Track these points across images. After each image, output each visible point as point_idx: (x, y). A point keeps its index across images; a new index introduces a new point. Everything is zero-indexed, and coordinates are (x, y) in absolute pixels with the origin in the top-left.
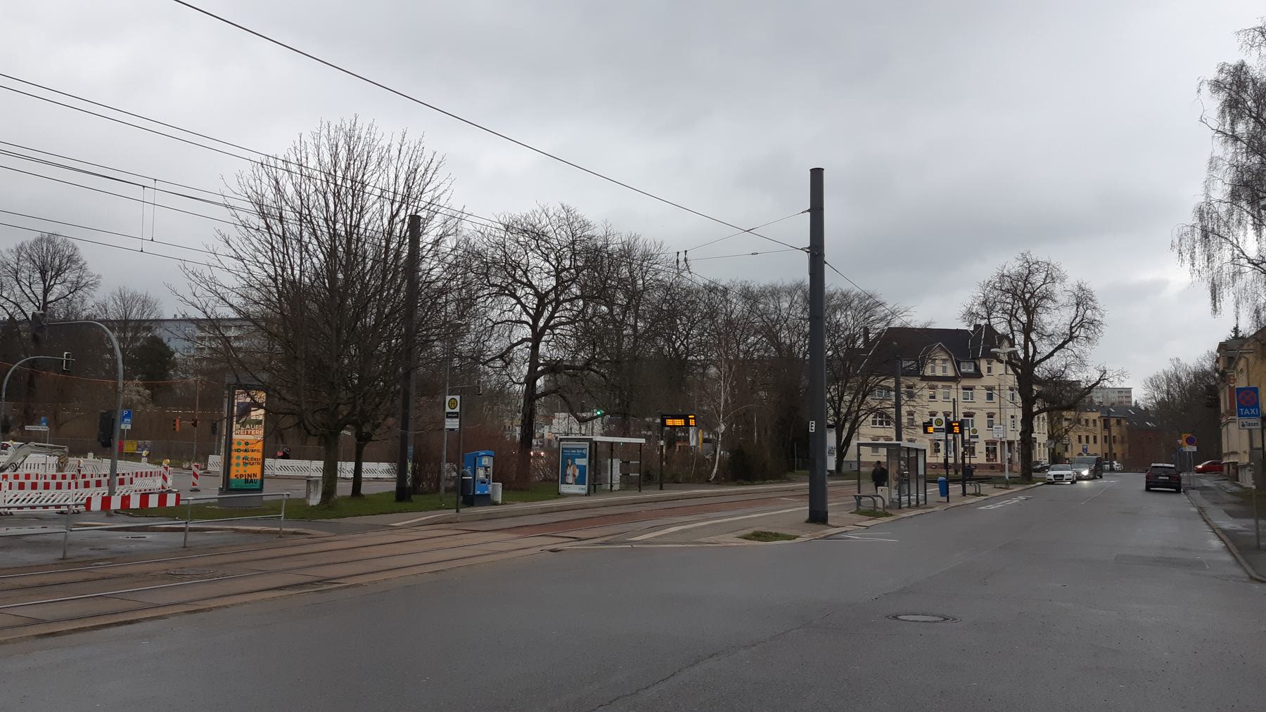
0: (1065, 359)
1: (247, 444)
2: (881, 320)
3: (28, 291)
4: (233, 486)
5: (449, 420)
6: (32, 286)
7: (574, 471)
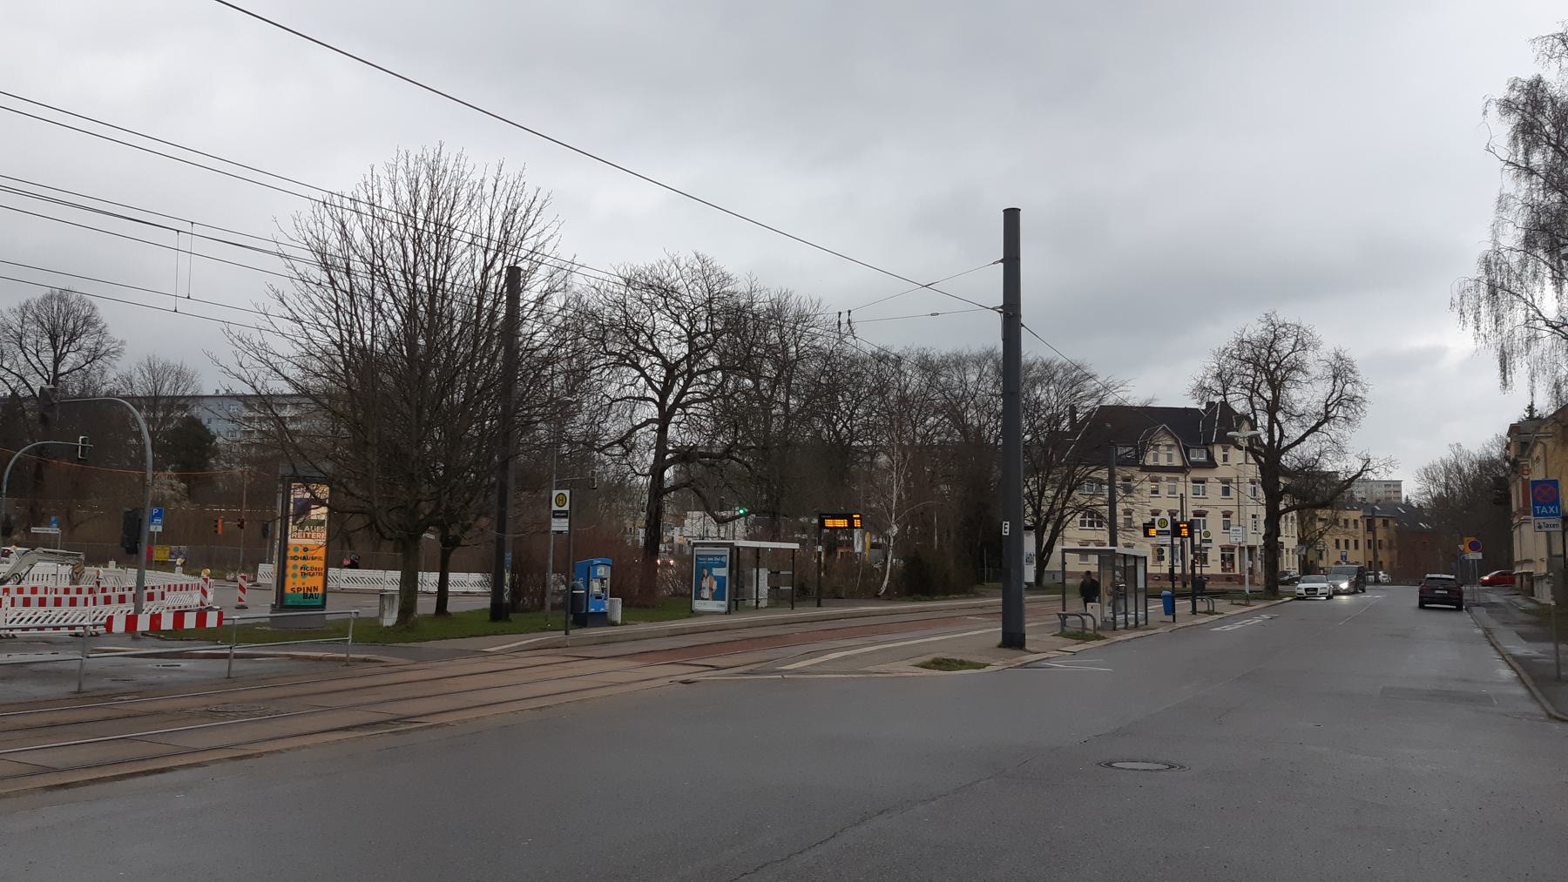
1: (306, 549)
2: (1092, 396)
3: (34, 360)
4: (289, 602)
5: (556, 520)
7: (711, 584)
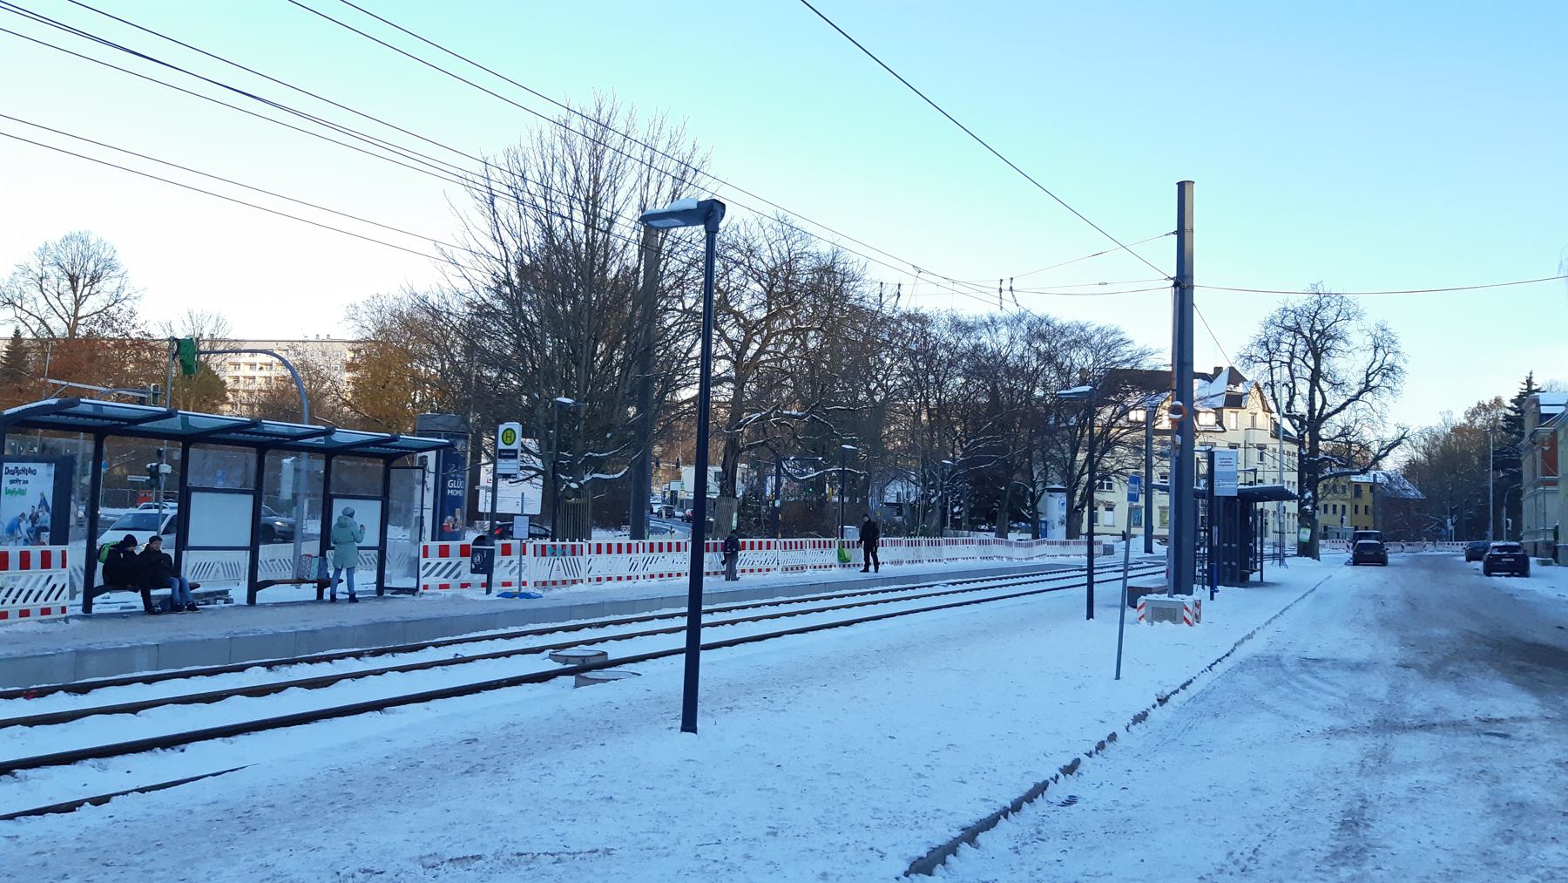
0: (1354, 414)
2: (1127, 361)
3: (55, 303)
6: (61, 297)
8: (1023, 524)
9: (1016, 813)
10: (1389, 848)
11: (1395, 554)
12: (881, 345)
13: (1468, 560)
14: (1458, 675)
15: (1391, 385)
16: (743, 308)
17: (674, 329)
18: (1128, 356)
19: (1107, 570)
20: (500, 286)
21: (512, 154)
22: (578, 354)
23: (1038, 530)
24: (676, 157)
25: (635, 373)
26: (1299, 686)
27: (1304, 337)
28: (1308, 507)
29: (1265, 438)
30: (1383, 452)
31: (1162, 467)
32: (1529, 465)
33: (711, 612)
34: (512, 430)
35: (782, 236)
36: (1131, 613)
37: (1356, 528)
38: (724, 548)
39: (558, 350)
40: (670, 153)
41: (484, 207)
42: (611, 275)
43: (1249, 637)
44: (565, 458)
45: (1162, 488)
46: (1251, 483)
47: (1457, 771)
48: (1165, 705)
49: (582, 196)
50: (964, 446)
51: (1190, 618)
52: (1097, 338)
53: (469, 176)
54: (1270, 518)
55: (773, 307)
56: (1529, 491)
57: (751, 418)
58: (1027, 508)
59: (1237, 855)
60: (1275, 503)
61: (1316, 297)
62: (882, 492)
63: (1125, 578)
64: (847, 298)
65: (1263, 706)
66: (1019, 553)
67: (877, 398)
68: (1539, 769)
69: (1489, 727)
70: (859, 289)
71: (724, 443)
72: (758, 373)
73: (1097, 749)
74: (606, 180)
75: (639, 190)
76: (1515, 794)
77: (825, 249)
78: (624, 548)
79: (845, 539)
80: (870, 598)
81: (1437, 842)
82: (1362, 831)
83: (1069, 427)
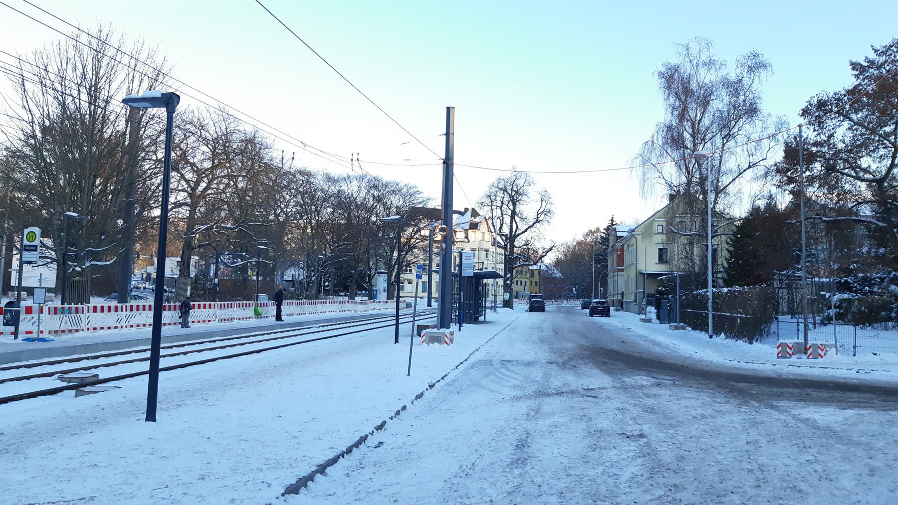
2: (420, 203)
8: (364, 292)
9: (349, 454)
10: (539, 457)
11: (549, 306)
12: (283, 188)
13: (583, 309)
14: (575, 367)
15: (549, 220)
16: (196, 160)
17: (149, 172)
18: (421, 200)
19: (408, 316)
20: (28, 139)
21: (38, 54)
22: (81, 188)
23: (372, 295)
24: (152, 65)
25: (122, 197)
26: (500, 375)
27: (508, 193)
28: (508, 282)
29: (488, 246)
30: (544, 254)
31: (436, 260)
32: (611, 261)
33: (145, 351)
34: (34, 233)
35: (222, 119)
36: (417, 339)
37: (531, 293)
38: (181, 308)
39: (68, 182)
40: (148, 62)
41: (17, 87)
42: (106, 136)
43: (477, 350)
44: (73, 251)
45: (437, 272)
46: (481, 269)
47: (572, 416)
48: (433, 389)
49: (87, 85)
50: (332, 248)
51: (448, 341)
52: (405, 190)
53: (7, 67)
54: (490, 288)
55: (216, 161)
56: (611, 274)
57: (200, 229)
58: (366, 283)
59: (464, 467)
60: (492, 280)
61: (514, 173)
62: (283, 274)
63: (414, 321)
64: (262, 159)
65: (481, 386)
66: (361, 308)
67: (281, 219)
68: (609, 413)
69: (590, 393)
70: (270, 154)
71: (182, 244)
72: (206, 201)
73: (396, 415)
74: (104, 75)
75: (127, 84)
76: (598, 426)
77: (249, 129)
78: (113, 309)
79: (259, 302)
80: (273, 336)
81: (562, 453)
82: (526, 449)
83: (389, 238)
